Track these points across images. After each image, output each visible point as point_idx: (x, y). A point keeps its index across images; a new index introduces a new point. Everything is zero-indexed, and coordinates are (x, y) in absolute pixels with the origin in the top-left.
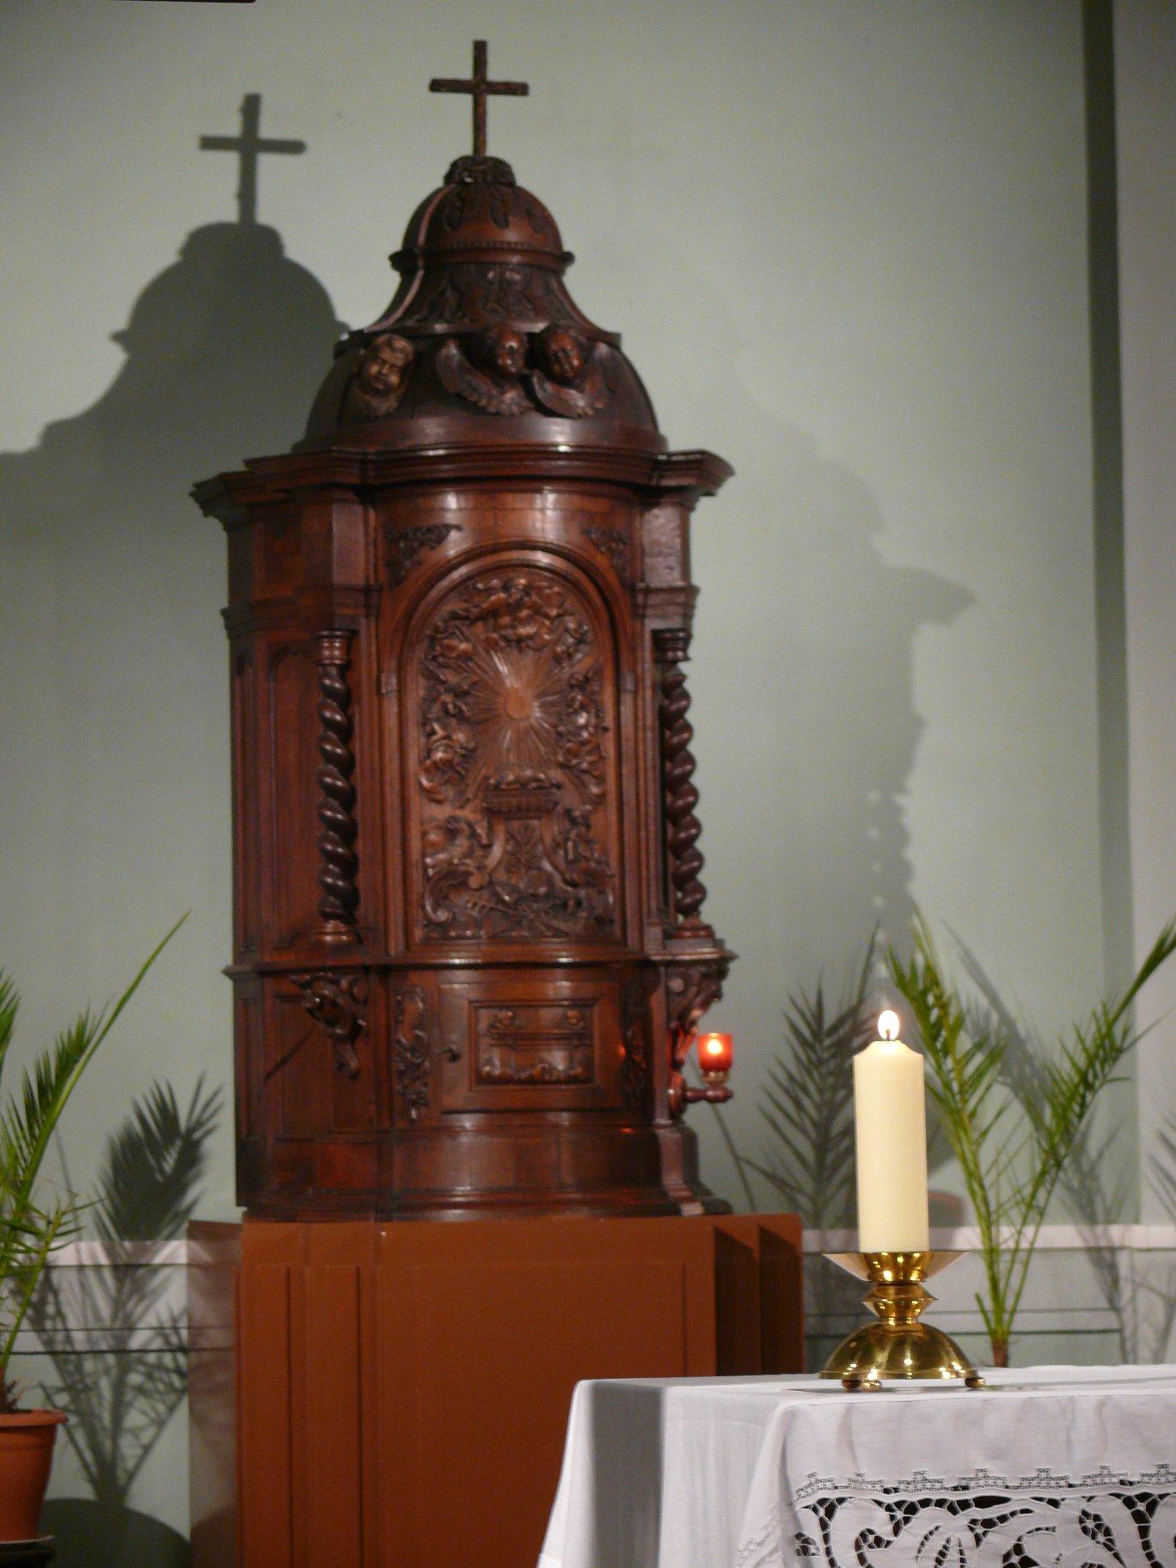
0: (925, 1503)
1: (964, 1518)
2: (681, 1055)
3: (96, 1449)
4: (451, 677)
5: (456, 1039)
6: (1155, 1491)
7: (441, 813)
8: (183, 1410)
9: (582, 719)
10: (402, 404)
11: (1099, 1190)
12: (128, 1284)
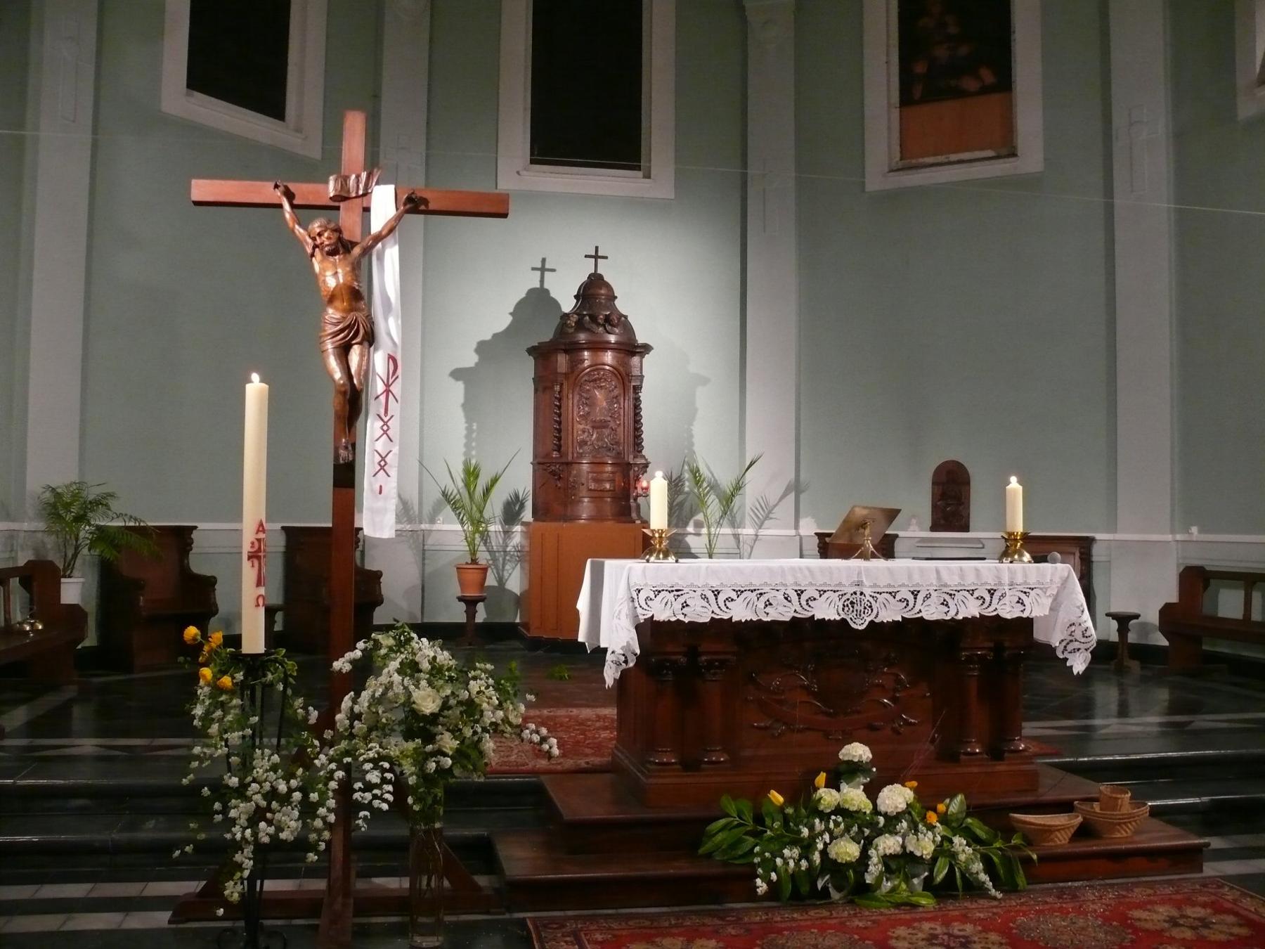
0: (663, 590)
1: (672, 594)
2: (637, 485)
3: (498, 573)
4: (584, 395)
5: (583, 480)
6: (719, 589)
7: (581, 427)
8: (519, 565)
9: (615, 406)
10: (575, 329)
11: (736, 520)
12: (507, 536)
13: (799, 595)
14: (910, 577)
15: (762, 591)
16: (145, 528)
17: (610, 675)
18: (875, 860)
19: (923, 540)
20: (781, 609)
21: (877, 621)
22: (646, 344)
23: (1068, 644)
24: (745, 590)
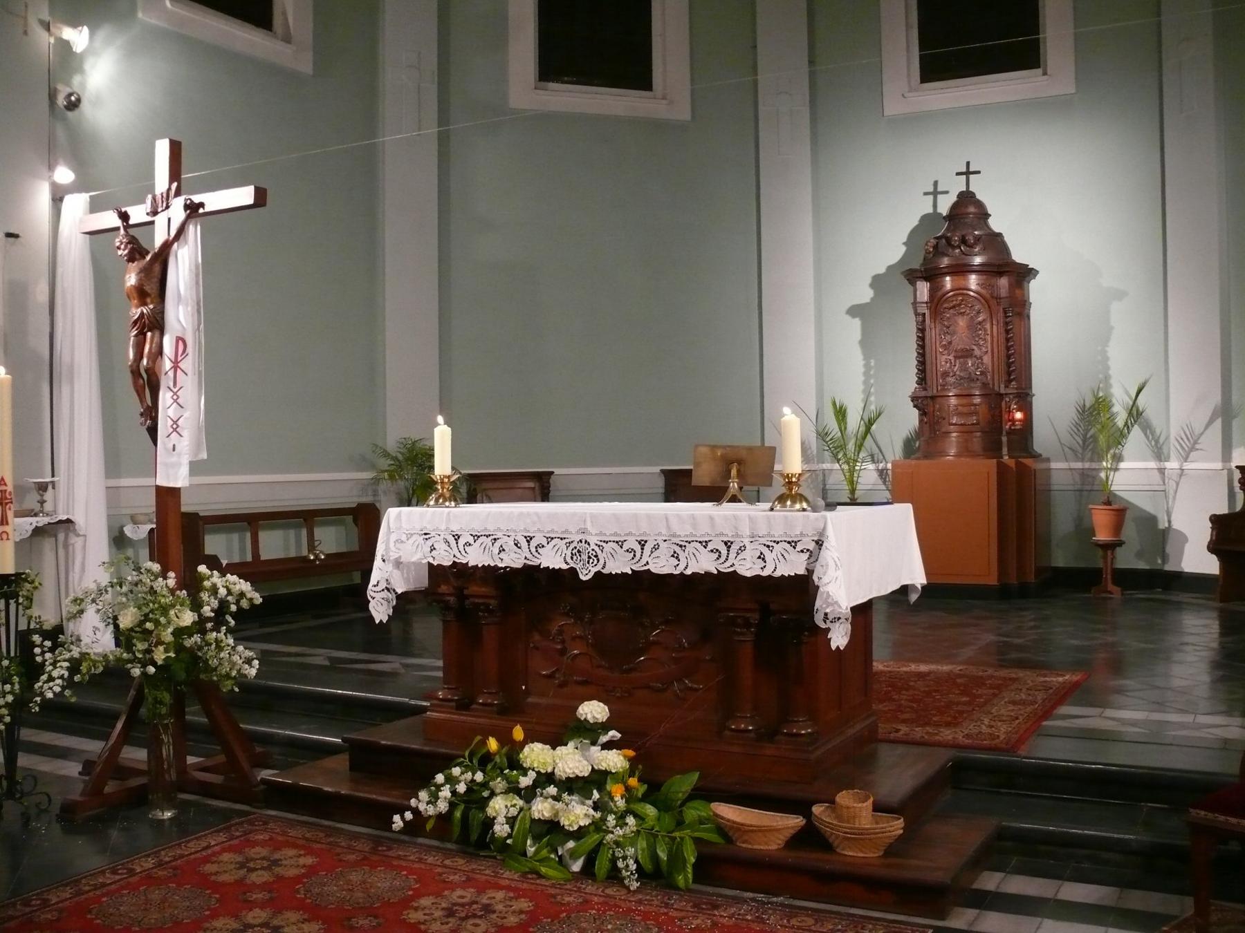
6: (459, 534)
13: (528, 541)
14: (694, 526)
15: (495, 537)
20: (513, 556)
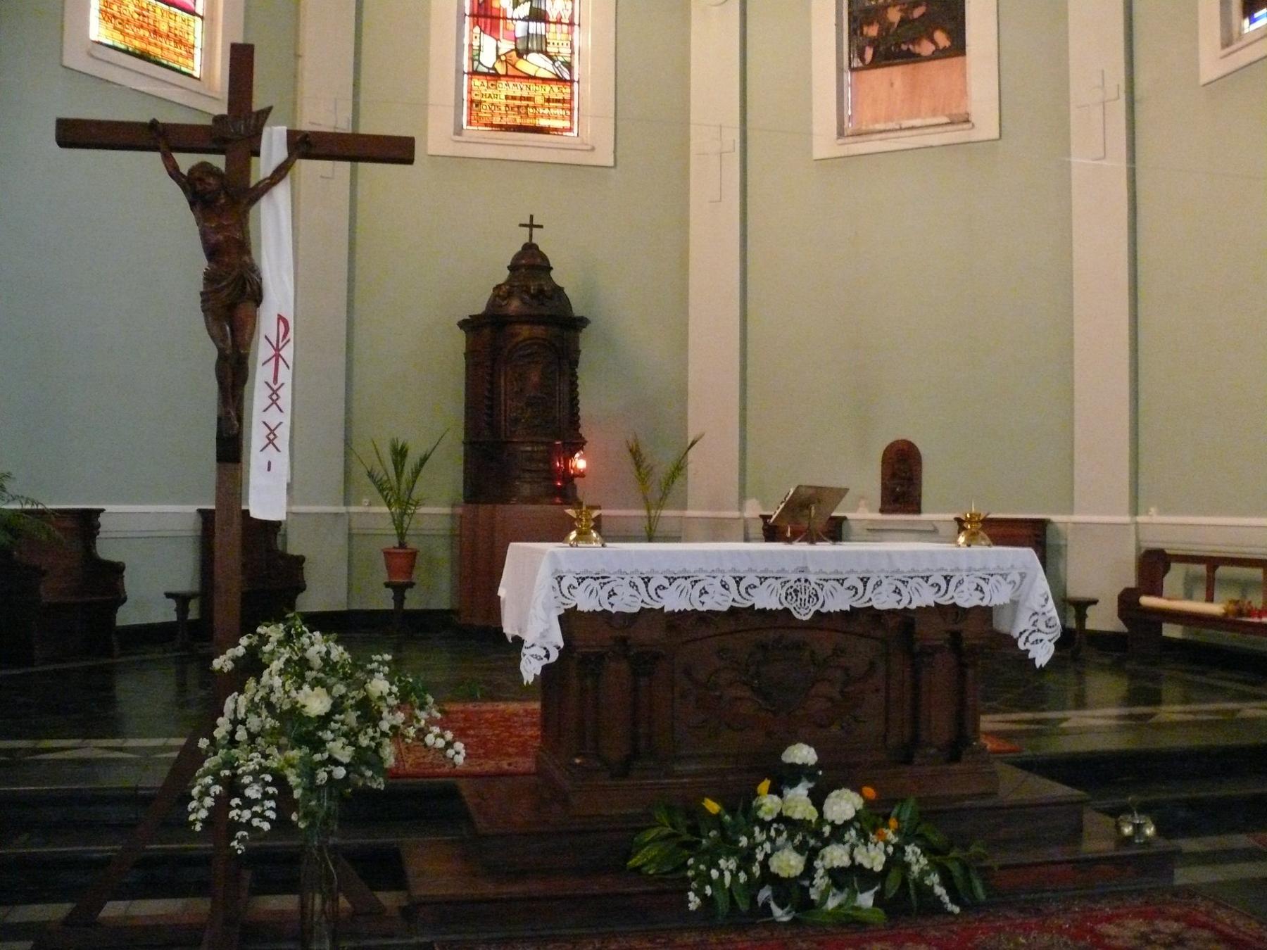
0: (587, 577)
1: (598, 581)
6: (650, 576)
15: (697, 579)
16: (42, 513)
17: (530, 669)
18: (821, 872)
19: (872, 521)
21: (824, 610)
22: (582, 317)
23: (1030, 634)
24: (679, 578)
